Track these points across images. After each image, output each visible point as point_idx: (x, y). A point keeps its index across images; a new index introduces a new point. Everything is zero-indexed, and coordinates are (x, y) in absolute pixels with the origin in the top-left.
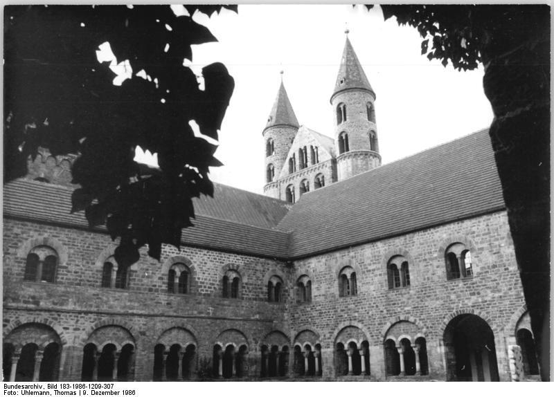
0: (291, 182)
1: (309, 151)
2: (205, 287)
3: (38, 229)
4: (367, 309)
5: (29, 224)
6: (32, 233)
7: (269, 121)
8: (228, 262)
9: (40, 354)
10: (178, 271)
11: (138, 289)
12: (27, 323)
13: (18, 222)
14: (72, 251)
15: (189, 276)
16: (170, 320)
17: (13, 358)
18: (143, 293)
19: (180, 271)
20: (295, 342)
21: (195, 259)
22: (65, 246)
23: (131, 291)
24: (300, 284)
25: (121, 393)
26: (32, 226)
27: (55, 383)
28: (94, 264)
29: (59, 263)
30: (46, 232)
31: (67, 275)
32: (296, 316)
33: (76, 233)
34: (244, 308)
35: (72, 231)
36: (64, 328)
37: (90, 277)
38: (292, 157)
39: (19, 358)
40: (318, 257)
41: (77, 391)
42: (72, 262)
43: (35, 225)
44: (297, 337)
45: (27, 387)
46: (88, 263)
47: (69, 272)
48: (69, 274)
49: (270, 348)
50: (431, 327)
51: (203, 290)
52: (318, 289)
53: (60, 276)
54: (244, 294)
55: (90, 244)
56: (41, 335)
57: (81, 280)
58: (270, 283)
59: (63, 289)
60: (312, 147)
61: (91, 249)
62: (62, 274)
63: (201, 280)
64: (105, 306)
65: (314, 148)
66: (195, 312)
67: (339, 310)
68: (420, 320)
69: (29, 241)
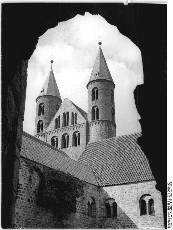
1: (70, 115)
7: (42, 91)
25: (171, 188)
27: (167, 207)
38: (58, 118)
41: (170, 204)
45: (169, 219)
60: (73, 113)
65: (74, 114)
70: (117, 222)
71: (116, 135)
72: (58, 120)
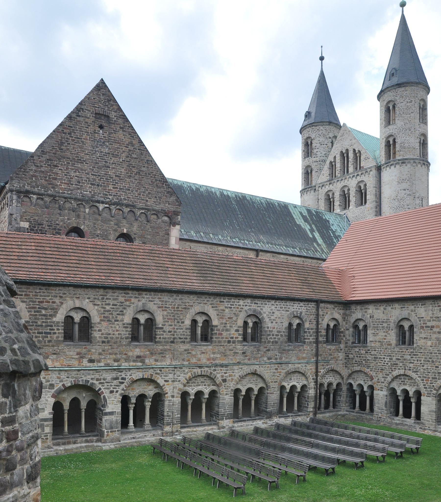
0: (331, 187)
1: (351, 155)
2: (273, 335)
3: (137, 296)
4: (422, 362)
5: (130, 292)
6: (133, 300)
8: (293, 310)
9: (149, 401)
11: (219, 342)
13: (121, 292)
14: (165, 313)
15: (259, 325)
17: (130, 406)
19: (252, 321)
21: (264, 310)
22: (159, 309)
23: (213, 344)
24: (356, 327)
26: (132, 294)
28: (183, 322)
29: (155, 325)
30: (144, 298)
31: (163, 335)
32: (351, 356)
33: (167, 295)
34: (306, 352)
35: (163, 294)
36: (165, 381)
37: (181, 335)
39: (134, 406)
42: (166, 323)
43: (135, 292)
44: (350, 375)
46: (178, 322)
47: (164, 332)
48: (165, 334)
49: (326, 385)
51: (271, 338)
52: (374, 335)
53: (158, 337)
54: (306, 339)
55: (178, 305)
57: (174, 339)
58: (328, 325)
59: (161, 347)
60: (354, 150)
61: (180, 309)
62: (159, 335)
63: (269, 329)
64: (194, 359)
65: (357, 152)
66: (265, 359)
67: (394, 358)
69: (131, 308)
72: (333, 164)
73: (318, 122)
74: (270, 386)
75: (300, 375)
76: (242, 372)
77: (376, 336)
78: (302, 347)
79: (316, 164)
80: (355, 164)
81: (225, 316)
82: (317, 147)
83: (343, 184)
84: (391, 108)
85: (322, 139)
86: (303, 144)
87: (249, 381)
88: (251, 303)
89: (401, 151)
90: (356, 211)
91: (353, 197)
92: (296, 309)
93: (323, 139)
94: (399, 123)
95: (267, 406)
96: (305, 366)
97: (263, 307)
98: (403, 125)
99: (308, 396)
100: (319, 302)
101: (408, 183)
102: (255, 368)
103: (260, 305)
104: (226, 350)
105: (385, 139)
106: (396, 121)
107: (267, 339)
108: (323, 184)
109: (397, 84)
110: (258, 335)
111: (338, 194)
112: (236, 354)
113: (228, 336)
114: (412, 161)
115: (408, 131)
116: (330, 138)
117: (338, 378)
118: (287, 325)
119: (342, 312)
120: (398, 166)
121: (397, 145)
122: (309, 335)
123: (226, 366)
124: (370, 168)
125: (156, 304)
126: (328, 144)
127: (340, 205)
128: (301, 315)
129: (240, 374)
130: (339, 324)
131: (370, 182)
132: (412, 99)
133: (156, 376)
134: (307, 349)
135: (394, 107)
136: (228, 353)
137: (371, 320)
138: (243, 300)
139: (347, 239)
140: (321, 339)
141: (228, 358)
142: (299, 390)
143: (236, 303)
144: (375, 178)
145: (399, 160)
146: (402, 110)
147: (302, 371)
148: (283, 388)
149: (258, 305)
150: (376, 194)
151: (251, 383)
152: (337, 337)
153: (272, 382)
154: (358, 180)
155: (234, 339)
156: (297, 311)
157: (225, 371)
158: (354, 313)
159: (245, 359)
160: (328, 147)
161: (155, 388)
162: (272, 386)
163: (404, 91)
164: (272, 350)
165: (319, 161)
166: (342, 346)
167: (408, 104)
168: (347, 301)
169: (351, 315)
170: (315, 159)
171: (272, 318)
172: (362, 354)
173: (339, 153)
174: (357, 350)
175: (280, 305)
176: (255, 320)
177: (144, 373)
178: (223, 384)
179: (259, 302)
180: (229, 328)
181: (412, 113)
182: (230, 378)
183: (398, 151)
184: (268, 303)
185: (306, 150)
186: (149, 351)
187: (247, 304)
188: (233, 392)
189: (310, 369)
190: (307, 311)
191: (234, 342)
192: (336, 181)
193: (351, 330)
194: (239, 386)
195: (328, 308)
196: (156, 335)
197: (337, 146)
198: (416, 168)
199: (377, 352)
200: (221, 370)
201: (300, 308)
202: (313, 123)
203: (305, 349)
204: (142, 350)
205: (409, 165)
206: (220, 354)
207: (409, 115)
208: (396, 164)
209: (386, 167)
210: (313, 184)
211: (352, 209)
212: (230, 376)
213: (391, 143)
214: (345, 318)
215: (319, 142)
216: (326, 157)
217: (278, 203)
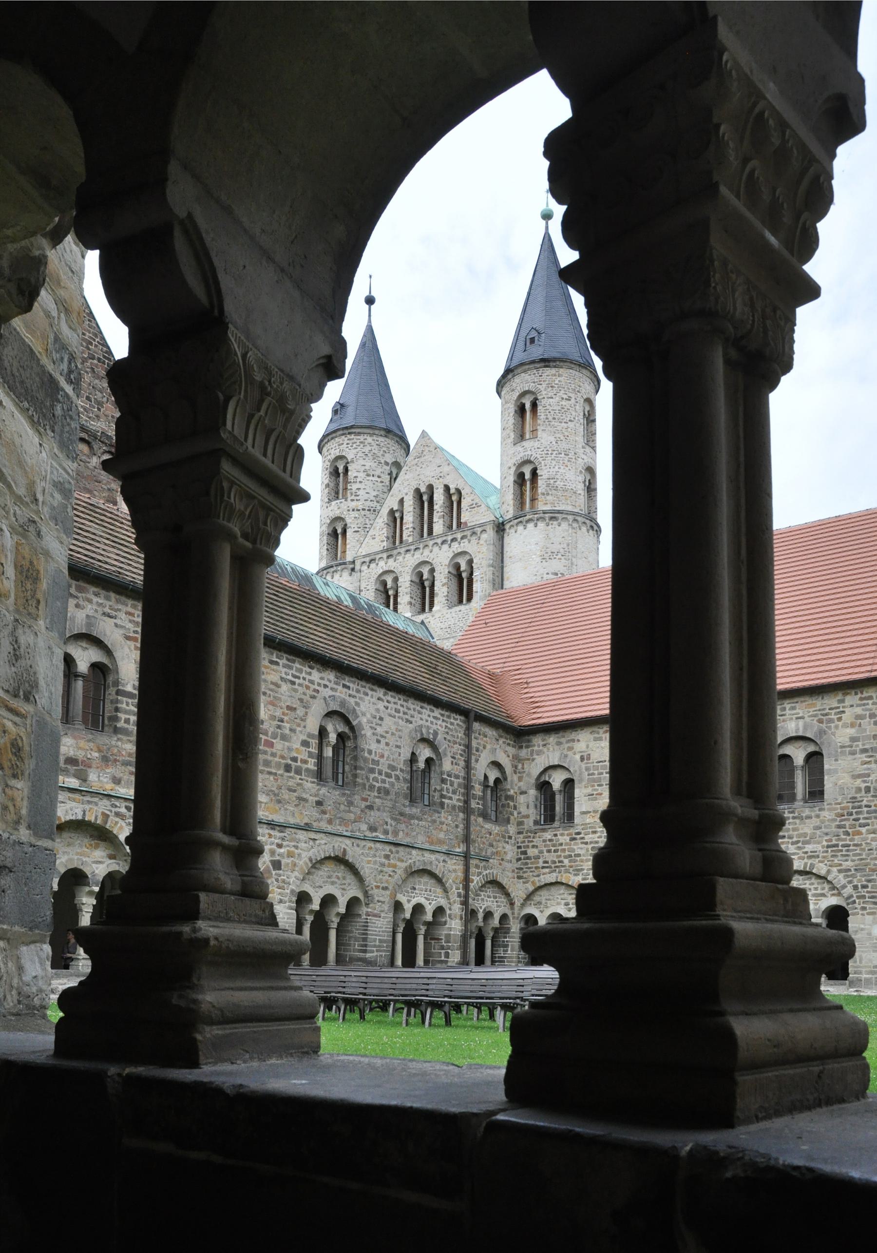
0: (391, 564)
1: (439, 497)
8: (421, 722)
10: (333, 729)
12: (71, 822)
16: (322, 839)
18: (275, 774)
20: (523, 905)
21: (363, 707)
22: (128, 642)
24: (544, 786)
29: (117, 683)
30: (90, 601)
32: (532, 852)
34: (444, 827)
40: (595, 729)
44: (529, 897)
50: (864, 887)
56: (724, 816)
60: (447, 488)
63: (373, 756)
65: (452, 491)
66: (364, 827)
68: (840, 871)
70: (574, 836)
71: (502, 585)
72: (397, 515)
73: (362, 427)
74: (372, 896)
75: (433, 881)
76: (314, 850)
77: (596, 799)
78: (437, 815)
79: (356, 514)
80: (446, 517)
81: (280, 699)
82: (358, 480)
83: (418, 557)
84: (528, 406)
85: (369, 464)
86: (327, 472)
87: (329, 877)
88: (336, 683)
89: (548, 494)
90: (448, 616)
91: (443, 585)
92: (427, 721)
93: (374, 465)
94: (545, 437)
95: (366, 946)
96: (444, 861)
97: (360, 698)
98: (554, 443)
99: (448, 936)
100: (472, 715)
101: (563, 561)
102: (343, 846)
103: (354, 693)
104: (280, 788)
105: (513, 469)
106: (540, 433)
107: (368, 779)
108: (372, 557)
109: (543, 360)
110: (347, 768)
111: (408, 578)
112: (302, 803)
113: (286, 753)
114: (571, 518)
115: (563, 455)
116: (387, 463)
117: (502, 902)
118: (409, 756)
119: (511, 751)
120: (541, 525)
121: (541, 482)
122: (451, 789)
123: (282, 827)
124: (482, 525)
125: (122, 627)
126: (382, 475)
127: (410, 603)
128: (435, 739)
129: (311, 854)
130: (506, 779)
131: (481, 556)
132: (570, 395)
133: (117, 823)
134: (446, 822)
135: (534, 405)
136: (285, 795)
137: (583, 766)
138: (318, 670)
139: (487, 621)
140: (473, 804)
141: (286, 809)
142: (429, 917)
143: (304, 675)
144: (491, 547)
145: (545, 512)
146: (552, 412)
147: (437, 872)
148: (398, 907)
149: (351, 692)
150: (494, 580)
151: (333, 883)
152: (501, 809)
153: (378, 887)
154: (455, 550)
155: (299, 764)
156: (428, 728)
157: (279, 841)
158: (539, 753)
159: (321, 819)
160: (382, 482)
161: (111, 857)
162: (377, 898)
163: (555, 375)
164: (378, 810)
165: (364, 510)
166: (512, 829)
167: (564, 403)
168: (524, 726)
169: (533, 760)
170: (353, 504)
171: (379, 730)
172: (561, 844)
173: (411, 493)
174: (548, 835)
175: (395, 703)
176: (342, 728)
177: (87, 807)
178: (274, 873)
179: (354, 685)
180: (287, 732)
181: (570, 421)
182: (290, 860)
183: (543, 494)
184: (370, 693)
185: (332, 485)
186: (100, 751)
187: (328, 683)
188: (294, 899)
189: (452, 870)
190: (447, 733)
191: (298, 771)
192: (403, 550)
193: (533, 792)
194: (307, 888)
195: (486, 736)
196: (117, 710)
197: (407, 477)
198: (579, 532)
199: (599, 834)
200: (270, 836)
201: (435, 721)
202: (352, 427)
203: (443, 820)
204: (82, 743)
205: (564, 525)
206: (268, 795)
207: (565, 425)
208: (538, 520)
209: (517, 524)
210: (349, 558)
211: (439, 611)
212: (290, 855)
213: (528, 476)
214: (516, 767)
215: (363, 468)
216: (378, 502)
217: (292, 568)
